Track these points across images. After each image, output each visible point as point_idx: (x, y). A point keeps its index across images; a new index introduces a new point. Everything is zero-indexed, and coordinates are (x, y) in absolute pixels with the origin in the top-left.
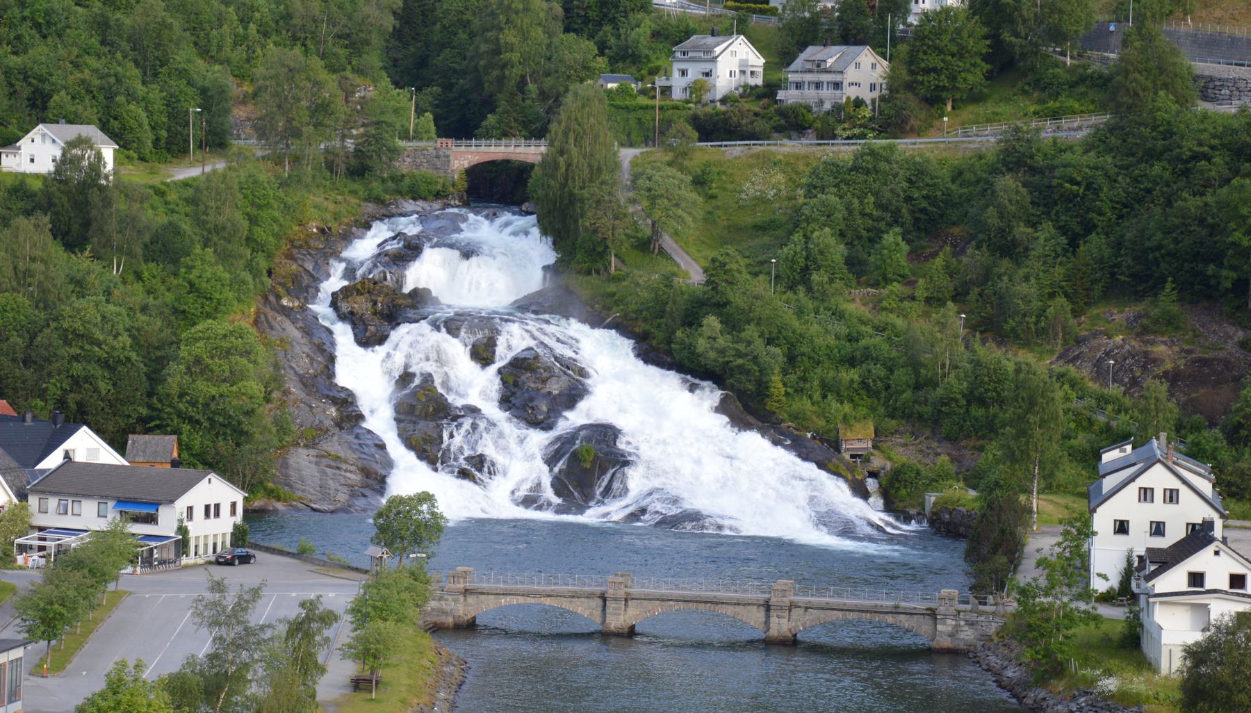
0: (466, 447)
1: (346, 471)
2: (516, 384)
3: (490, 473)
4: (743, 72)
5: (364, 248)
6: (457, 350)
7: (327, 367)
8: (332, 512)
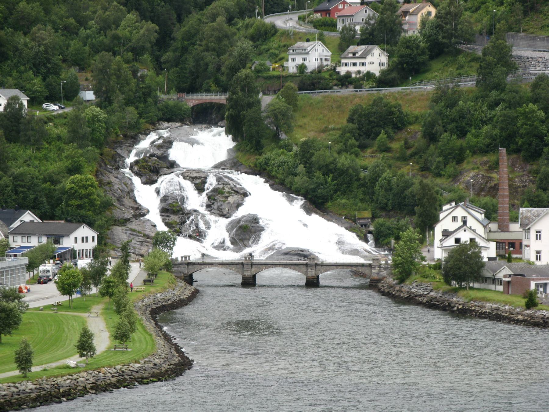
4: (321, 59)
5: (145, 144)
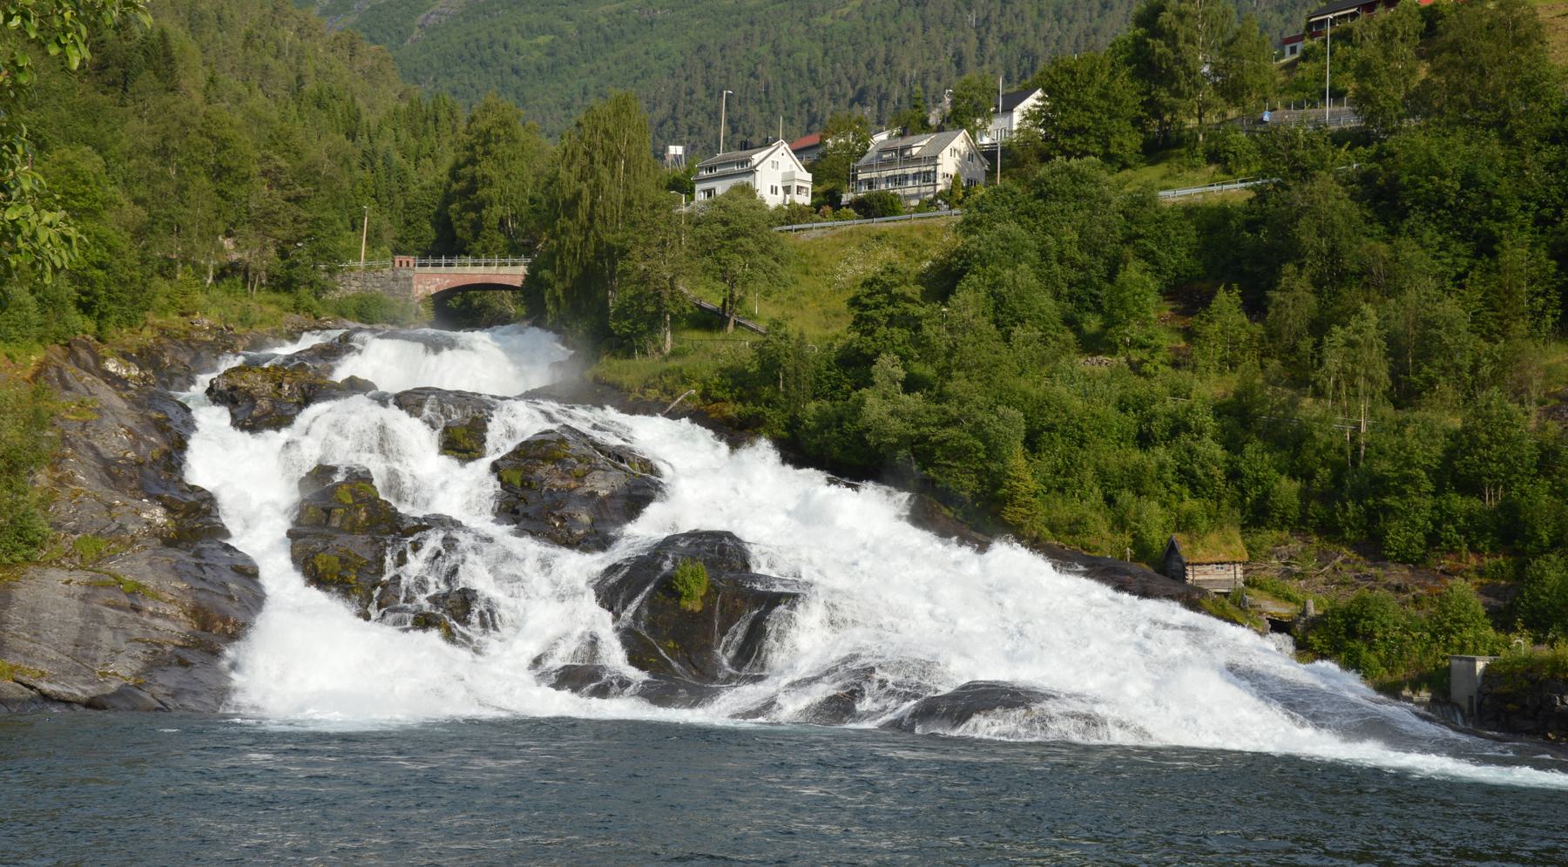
0: (431, 579)
1: (153, 615)
2: (527, 484)
3: (484, 624)
4: (787, 190)
6: (417, 441)
7: (168, 455)
8: (92, 704)
